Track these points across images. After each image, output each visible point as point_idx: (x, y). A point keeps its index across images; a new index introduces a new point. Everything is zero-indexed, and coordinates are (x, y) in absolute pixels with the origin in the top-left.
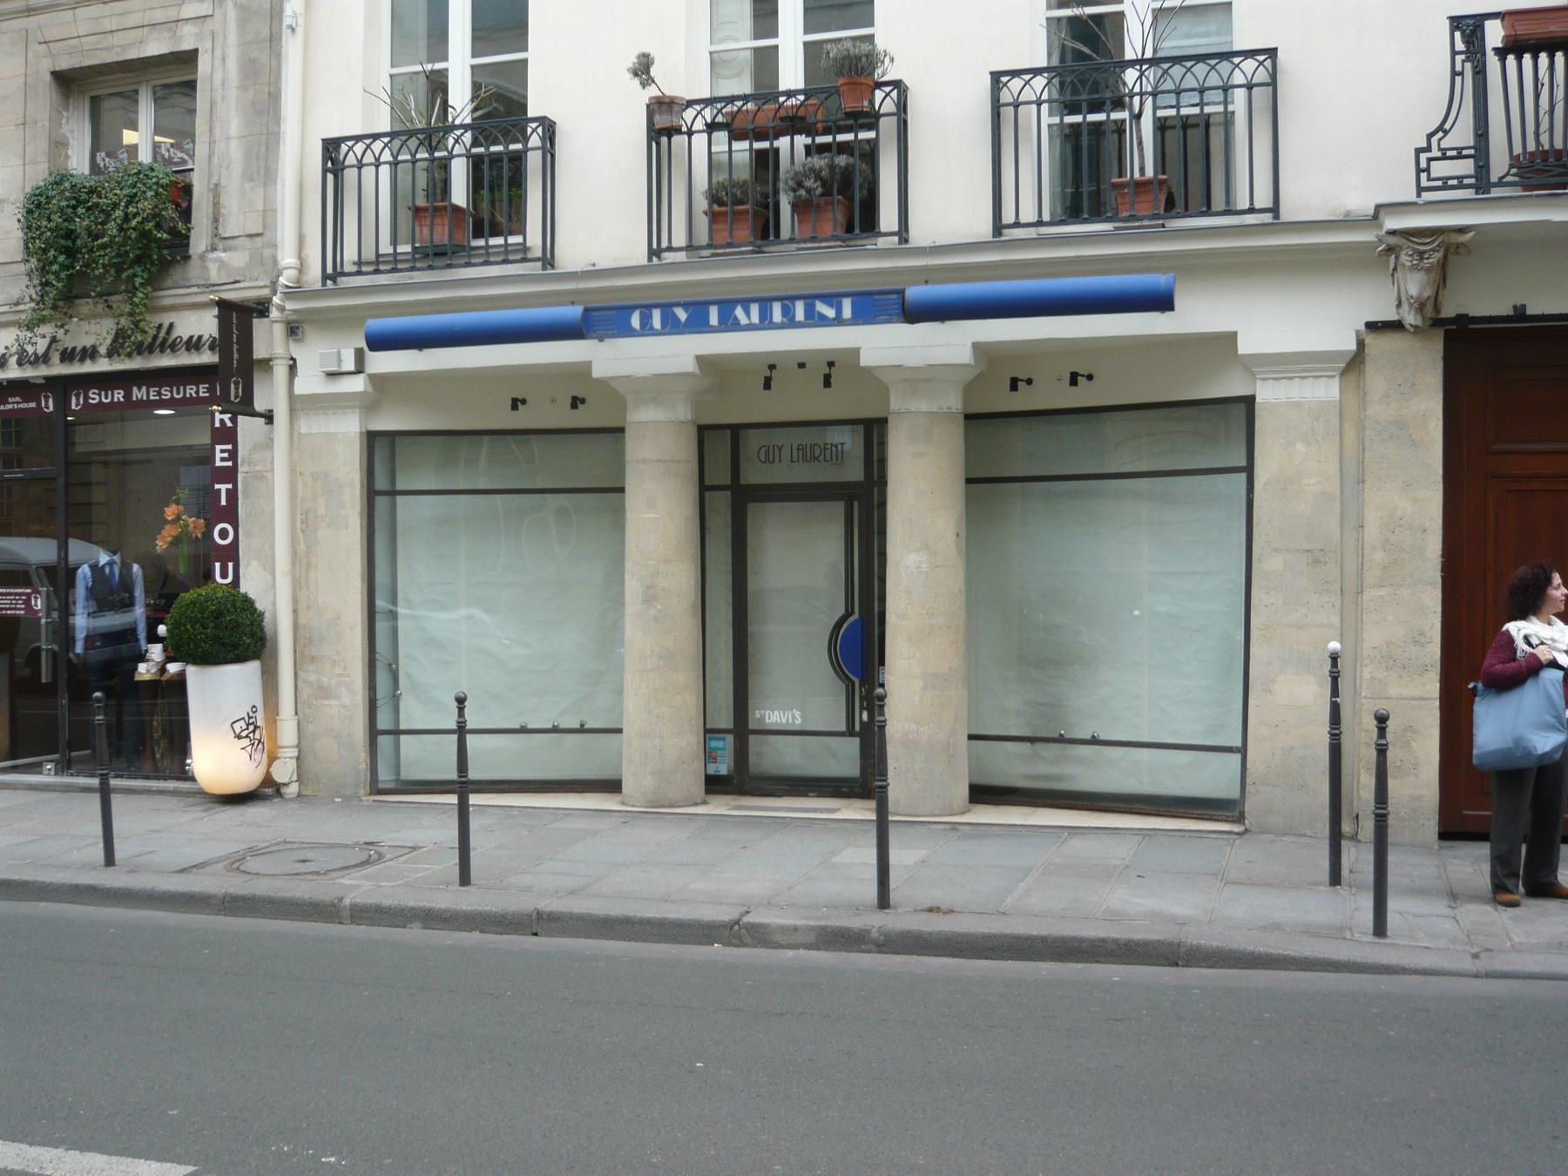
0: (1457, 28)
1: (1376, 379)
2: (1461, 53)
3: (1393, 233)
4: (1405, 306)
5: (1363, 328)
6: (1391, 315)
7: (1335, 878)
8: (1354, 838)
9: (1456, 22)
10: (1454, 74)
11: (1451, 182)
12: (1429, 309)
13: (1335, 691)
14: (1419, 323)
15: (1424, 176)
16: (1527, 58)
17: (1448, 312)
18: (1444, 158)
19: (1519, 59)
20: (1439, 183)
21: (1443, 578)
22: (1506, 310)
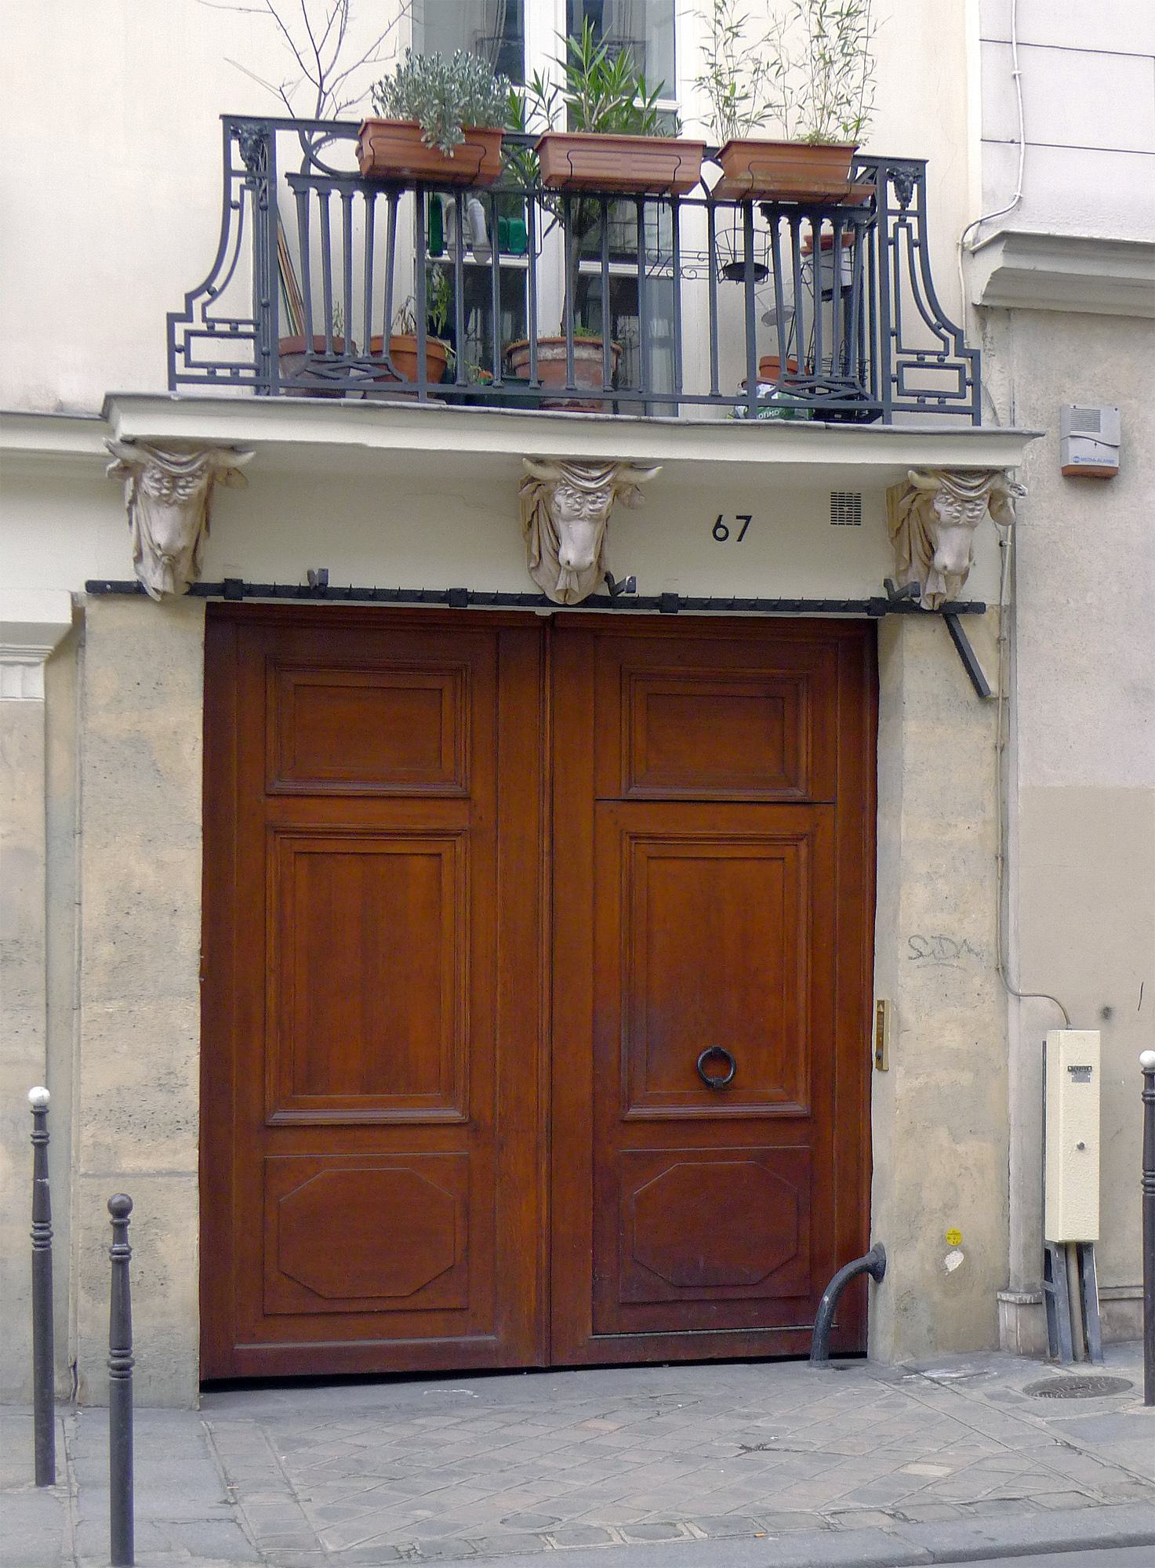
0: (235, 133)
1: (101, 669)
2: (239, 174)
3: (131, 442)
4: (148, 560)
5: (81, 589)
6: (125, 573)
7: (45, 1473)
8: (70, 1400)
9: (233, 125)
10: (228, 205)
11: (220, 373)
12: (184, 567)
13: (41, 1168)
14: (169, 588)
15: (180, 358)
16: (381, 198)
17: (212, 574)
18: (211, 333)
19: (370, 199)
20: (203, 372)
21: (203, 986)
22: (295, 577)
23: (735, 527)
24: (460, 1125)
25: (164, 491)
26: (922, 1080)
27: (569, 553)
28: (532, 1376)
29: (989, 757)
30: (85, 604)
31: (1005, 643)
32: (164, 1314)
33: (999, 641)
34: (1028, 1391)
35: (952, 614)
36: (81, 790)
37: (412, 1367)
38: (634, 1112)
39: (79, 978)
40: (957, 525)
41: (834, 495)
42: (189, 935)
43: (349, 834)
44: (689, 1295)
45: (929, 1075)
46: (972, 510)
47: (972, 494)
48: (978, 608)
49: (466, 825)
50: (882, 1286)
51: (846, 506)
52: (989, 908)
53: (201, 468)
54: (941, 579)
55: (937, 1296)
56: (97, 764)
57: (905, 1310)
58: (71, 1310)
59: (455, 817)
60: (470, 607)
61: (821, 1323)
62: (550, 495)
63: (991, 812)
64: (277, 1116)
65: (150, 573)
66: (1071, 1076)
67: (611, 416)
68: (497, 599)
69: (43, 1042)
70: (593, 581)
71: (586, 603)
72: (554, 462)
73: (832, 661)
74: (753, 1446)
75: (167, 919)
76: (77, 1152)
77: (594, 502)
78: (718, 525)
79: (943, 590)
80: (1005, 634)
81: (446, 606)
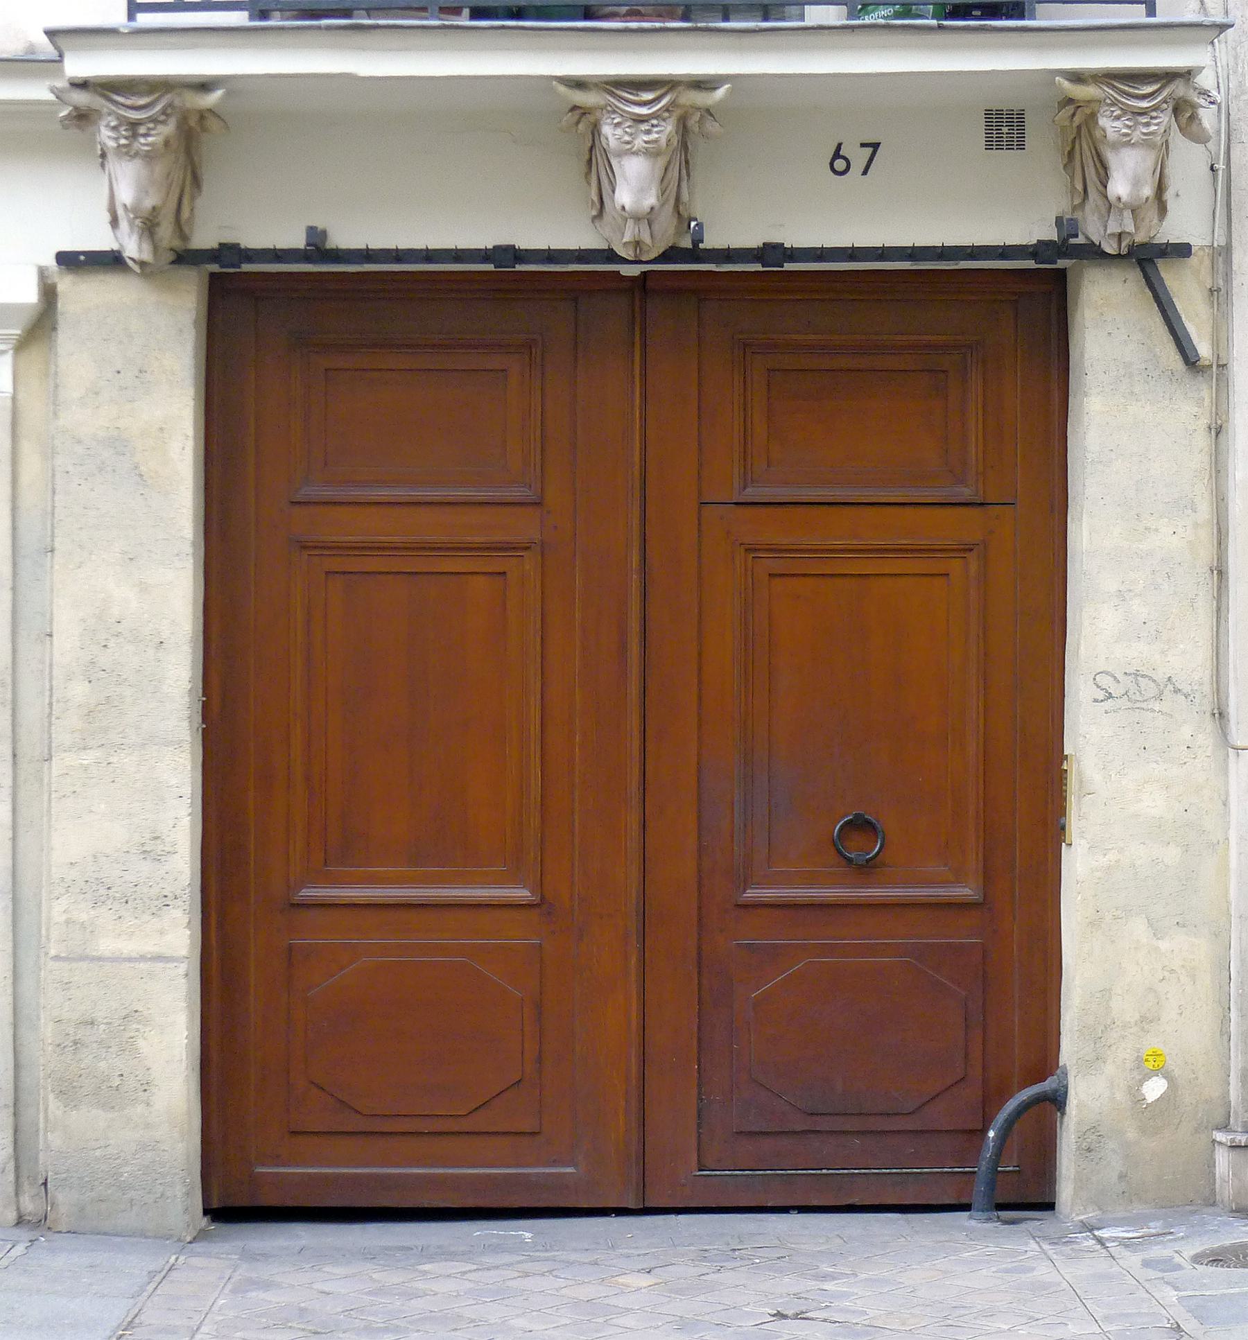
1: (74, 353)
3: (82, 85)
5: (51, 262)
6: (102, 241)
12: (166, 231)
14: (147, 256)
17: (205, 238)
22: (297, 241)
24: (530, 906)
25: (123, 141)
26: (1112, 856)
27: (624, 197)
28: (620, 1219)
29: (1202, 441)
30: (56, 280)
32: (148, 1126)
34: (1197, 1259)
35: (1148, 259)
37: (470, 1202)
38: (751, 894)
39: (50, 724)
40: (1128, 144)
41: (988, 113)
42: (177, 672)
43: (384, 549)
44: (825, 1124)
45: (1121, 851)
46: (1147, 125)
47: (1145, 104)
48: (1183, 250)
49: (537, 537)
50: (1066, 1118)
51: (1004, 127)
52: (1204, 635)
53: (164, 112)
54: (1127, 214)
55: (1131, 1135)
56: (70, 468)
57: (1089, 1150)
58: (41, 1116)
59: (525, 527)
60: (519, 268)
61: (983, 1166)
62: (1093, 117)
63: (1205, 510)
64: (305, 892)
65: (127, 238)
68: (550, 256)
69: (9, 800)
70: (671, 231)
71: (665, 257)
72: (596, 85)
73: (1009, 320)
74: (790, 1313)
75: (151, 652)
76: (48, 929)
77: (648, 132)
78: (837, 155)
79: (1130, 228)
81: (490, 267)
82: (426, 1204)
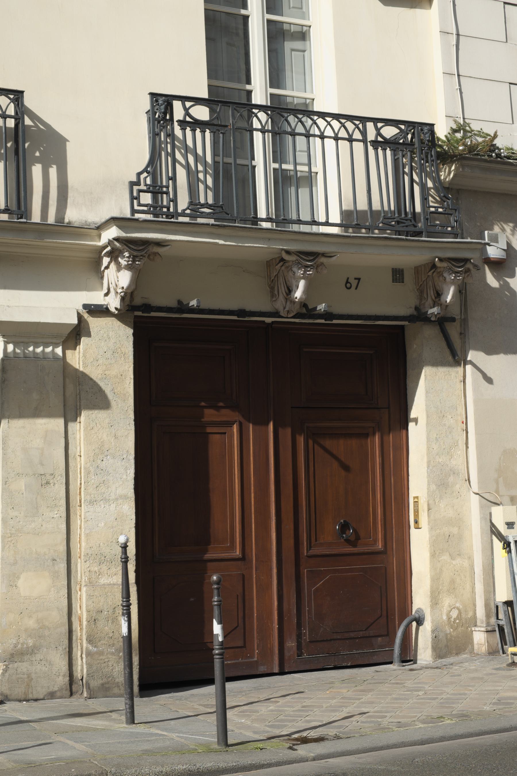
5: (81, 308)
20: (145, 208)
22: (173, 304)
23: (354, 283)
26: (438, 531)
31: (463, 334)
33: (461, 334)
36: (80, 402)
41: (393, 269)
48: (453, 320)
66: (506, 526)
67: (404, 237)
78: (347, 282)
80: (463, 332)
82: (245, 674)
